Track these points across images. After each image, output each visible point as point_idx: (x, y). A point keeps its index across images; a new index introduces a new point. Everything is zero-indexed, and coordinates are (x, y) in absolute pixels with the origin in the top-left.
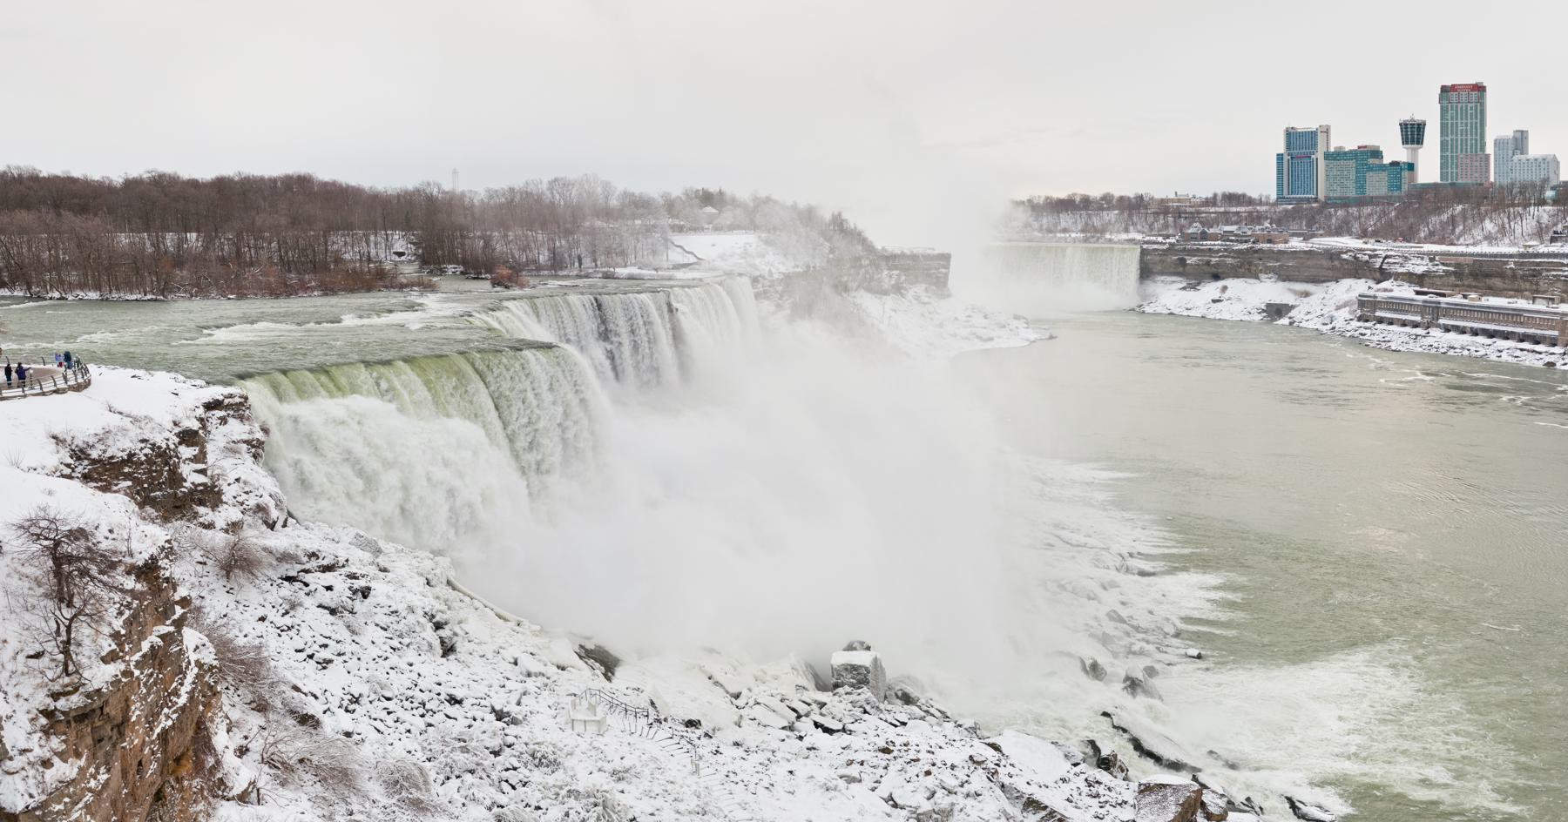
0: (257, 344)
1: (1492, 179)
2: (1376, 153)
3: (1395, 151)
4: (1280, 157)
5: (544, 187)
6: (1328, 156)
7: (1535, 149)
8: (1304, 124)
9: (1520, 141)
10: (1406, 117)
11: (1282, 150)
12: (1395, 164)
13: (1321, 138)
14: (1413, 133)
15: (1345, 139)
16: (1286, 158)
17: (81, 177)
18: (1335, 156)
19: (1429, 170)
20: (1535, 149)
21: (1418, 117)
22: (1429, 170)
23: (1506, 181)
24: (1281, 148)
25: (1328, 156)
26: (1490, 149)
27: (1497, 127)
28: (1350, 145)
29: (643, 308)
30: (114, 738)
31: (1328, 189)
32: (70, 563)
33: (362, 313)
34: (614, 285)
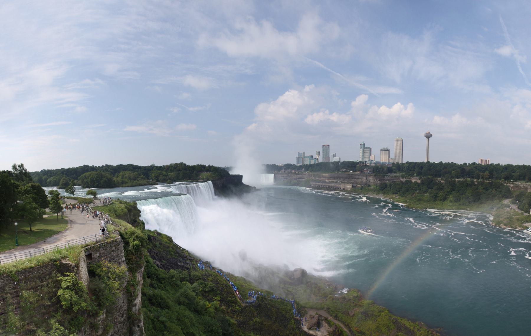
3: (315, 156)
12: (315, 158)
14: (319, 153)
19: (321, 160)
29: (194, 187)
33: (148, 189)
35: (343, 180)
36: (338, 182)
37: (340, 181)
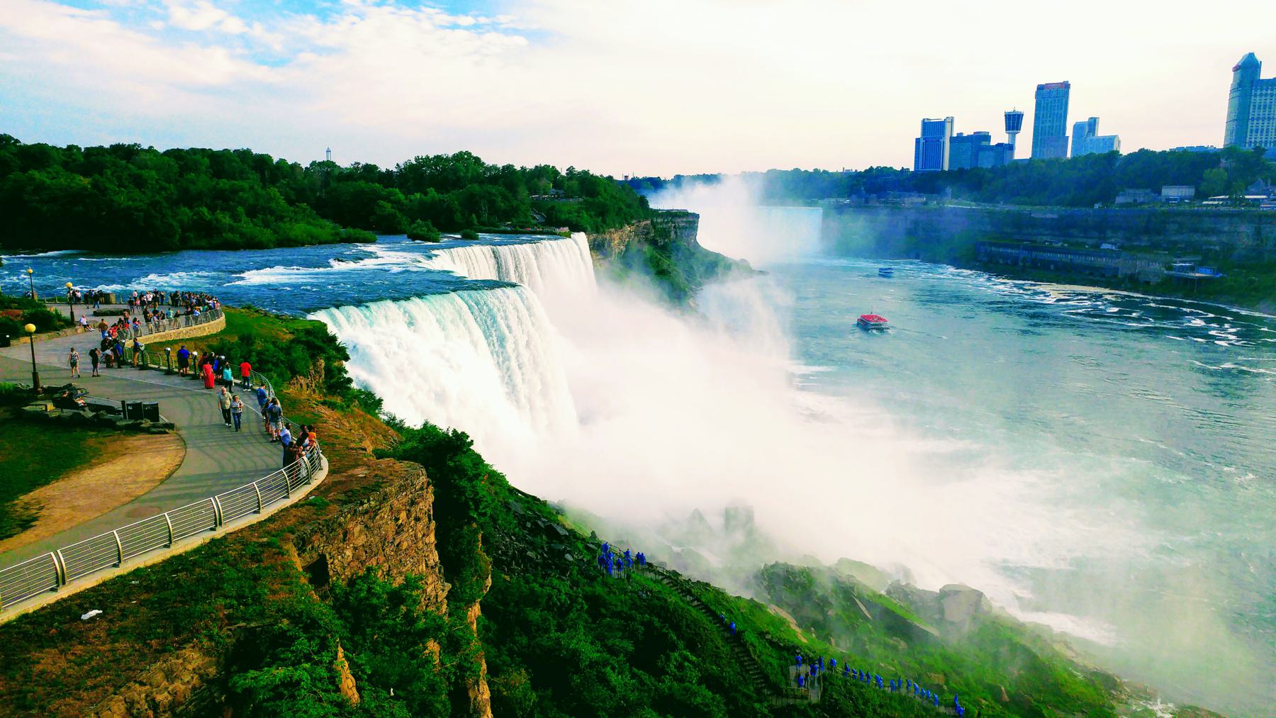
0: (313, 285)
1: (1069, 155)
2: (987, 137)
3: (999, 136)
4: (918, 141)
5: (677, 194)
6: (952, 139)
7: (1102, 131)
8: (936, 115)
9: (1093, 123)
10: (1010, 110)
11: (919, 136)
12: (999, 145)
13: (948, 126)
14: (1013, 121)
15: (963, 127)
16: (922, 141)
17: (598, 175)
18: (959, 140)
19: (1023, 149)
20: (1102, 131)
21: (1019, 110)
22: (1023, 149)
23: (1084, 153)
24: (918, 133)
25: (952, 139)
26: (1069, 132)
27: (1076, 114)
28: (968, 132)
30: (129, 622)
31: (950, 167)
32: (278, 376)
34: (351, 685)
35: (1129, 239)
36: (1105, 246)
37: (1113, 240)
